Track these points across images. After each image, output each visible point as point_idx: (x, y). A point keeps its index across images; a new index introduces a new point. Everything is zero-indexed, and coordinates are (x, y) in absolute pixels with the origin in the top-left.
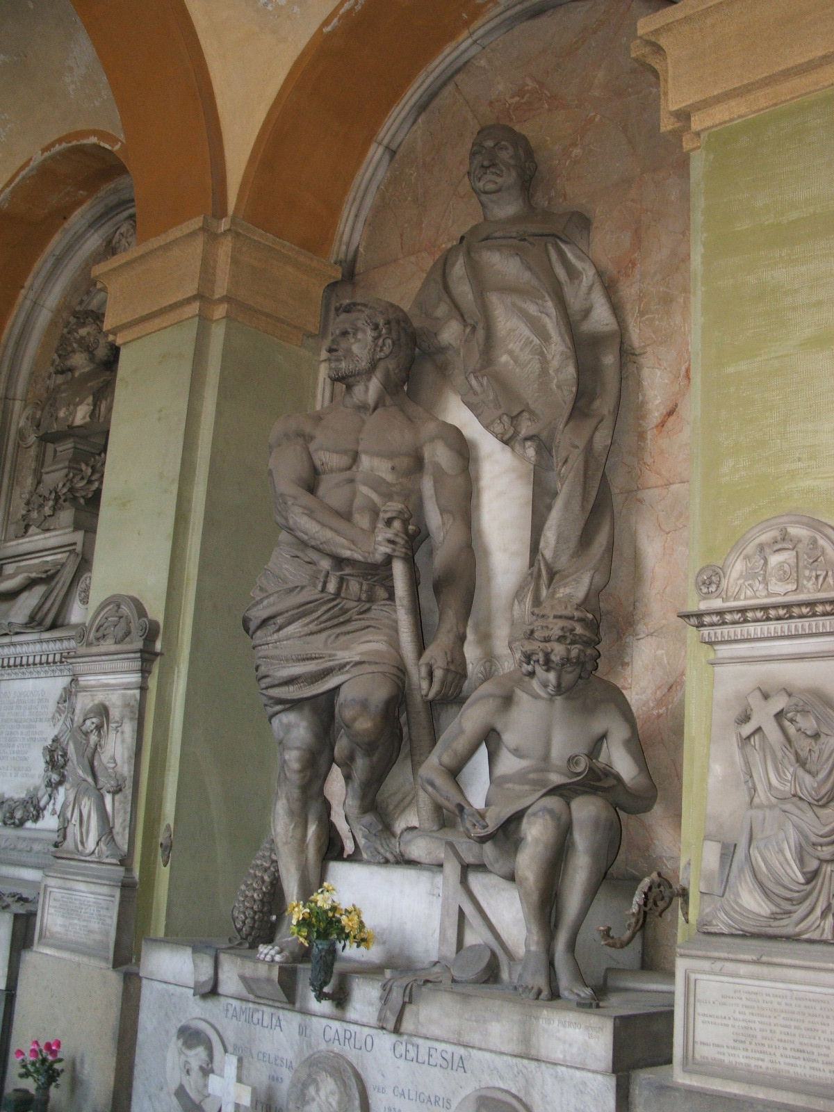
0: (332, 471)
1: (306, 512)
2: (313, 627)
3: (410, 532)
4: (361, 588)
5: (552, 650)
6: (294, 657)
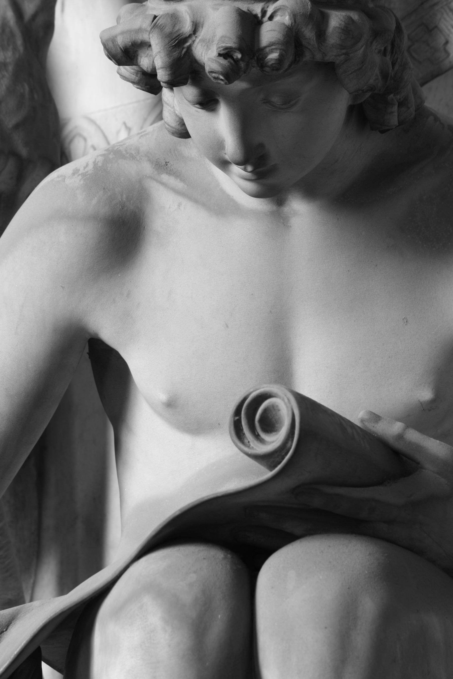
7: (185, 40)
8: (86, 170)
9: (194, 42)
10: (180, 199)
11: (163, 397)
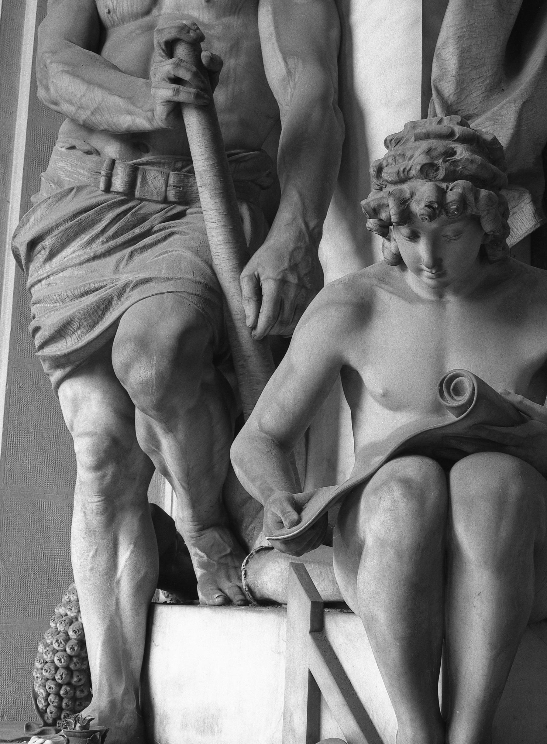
0: (123, 20)
1: (66, 68)
2: (98, 247)
3: (204, 61)
4: (167, 181)
5: (412, 195)
6: (69, 294)
7: (406, 201)
8: (345, 282)
9: (411, 202)
10: (391, 295)
11: (381, 391)
